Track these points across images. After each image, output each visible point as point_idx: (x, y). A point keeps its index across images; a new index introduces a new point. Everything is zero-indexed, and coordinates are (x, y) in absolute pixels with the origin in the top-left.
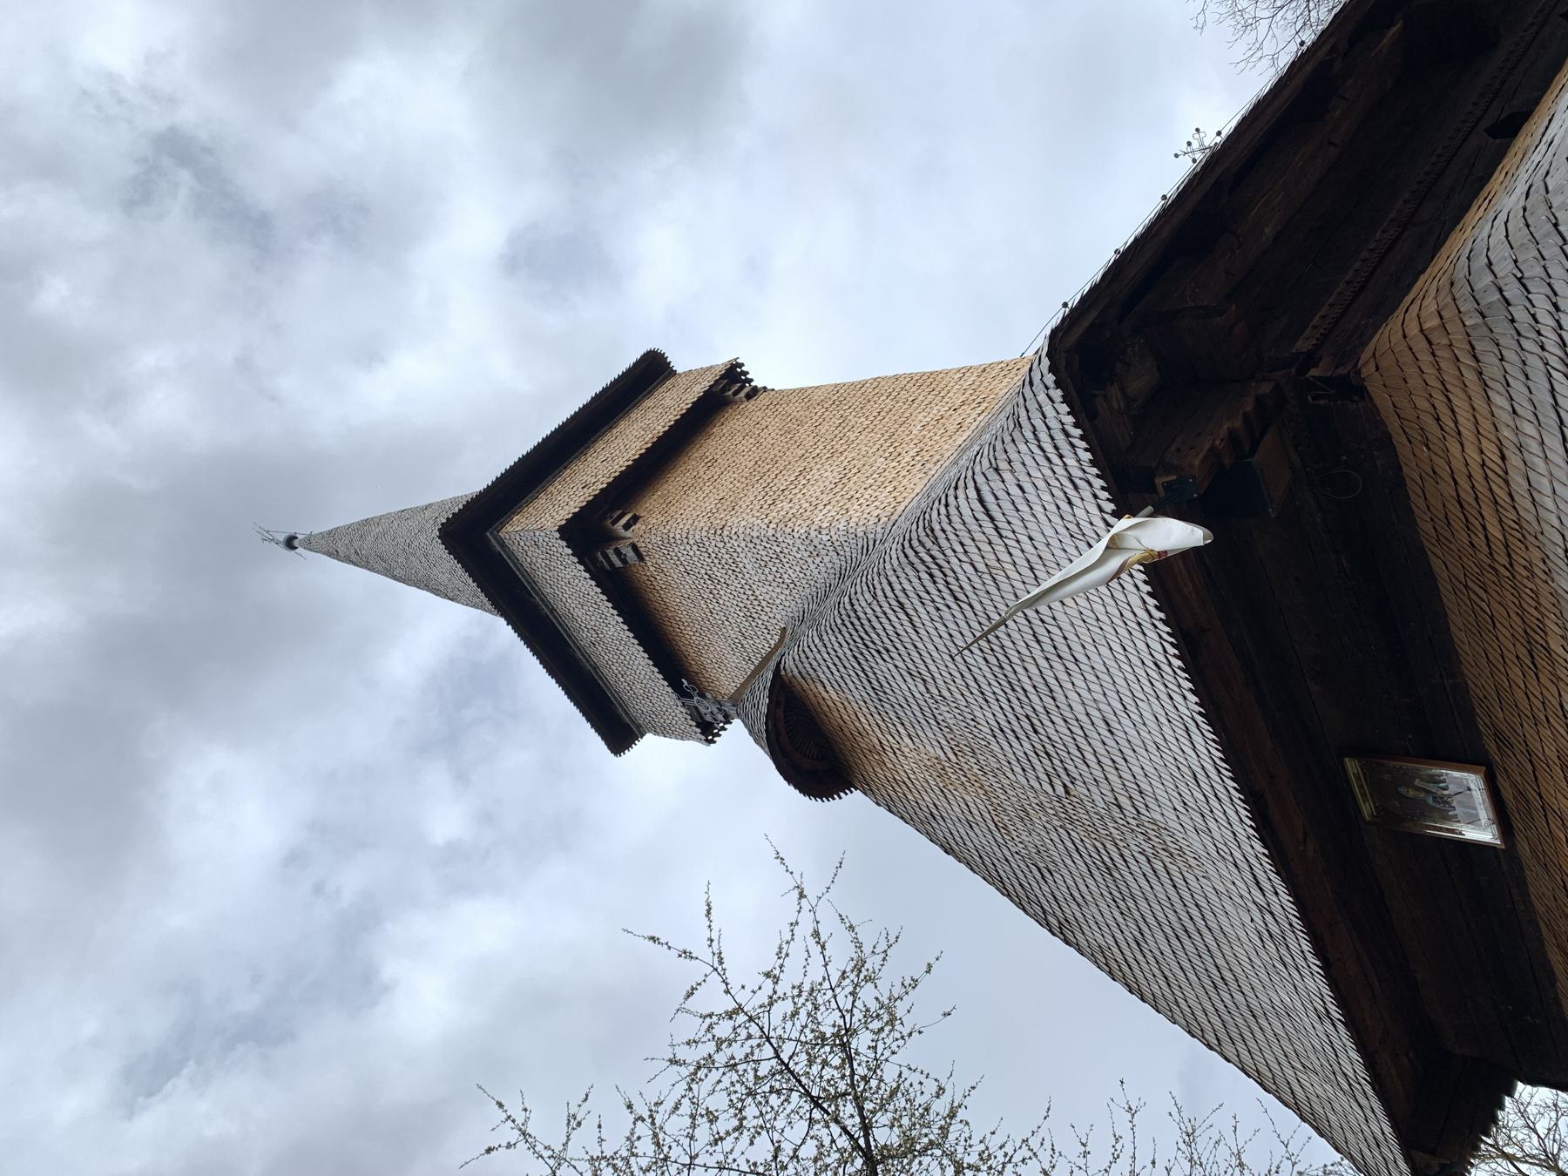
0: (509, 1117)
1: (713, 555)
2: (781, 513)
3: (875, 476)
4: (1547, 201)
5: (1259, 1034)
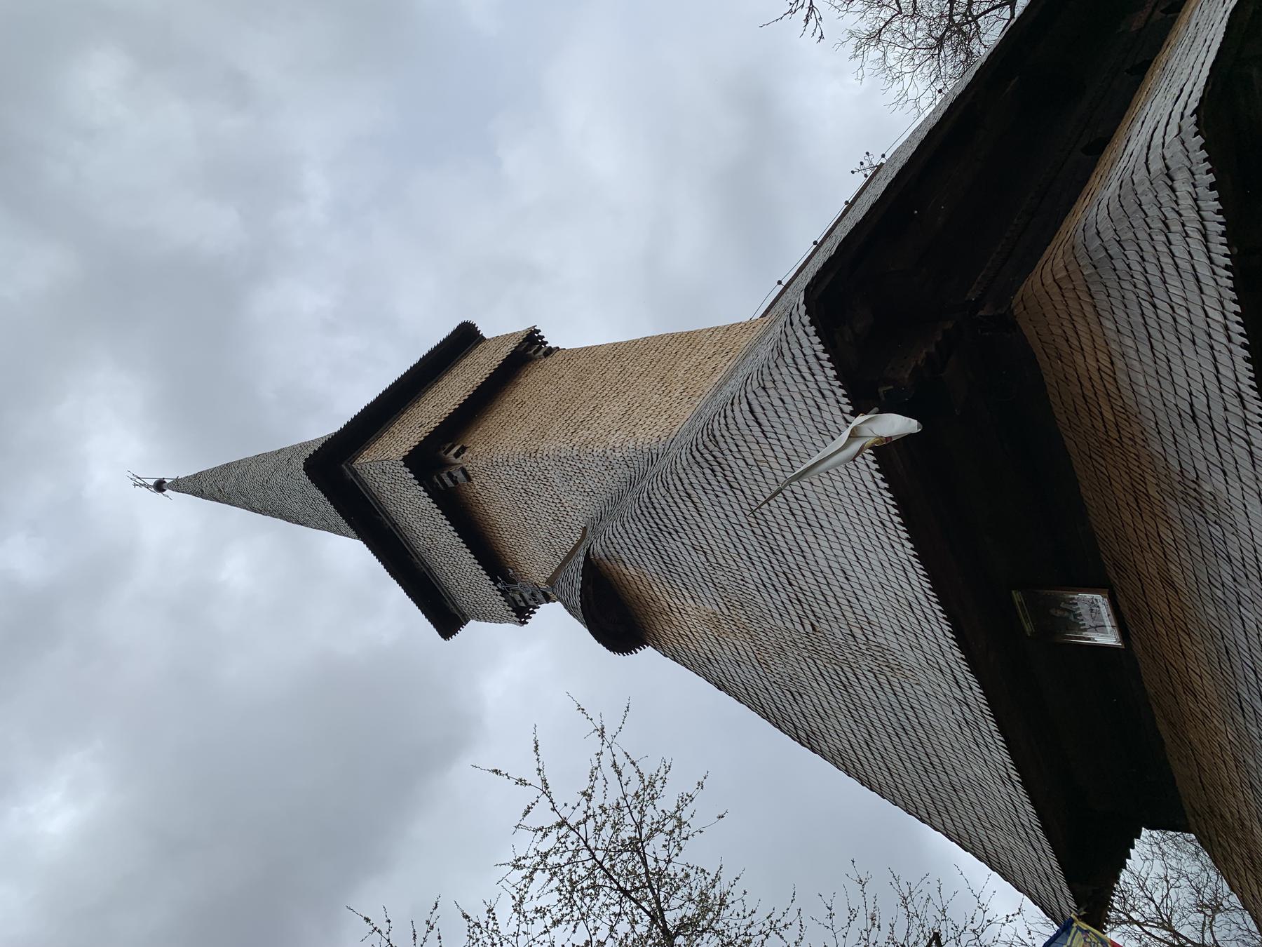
0: (375, 929)
1: (529, 473)
2: (582, 438)
3: (653, 408)
4: (1134, 190)
5: (958, 805)
